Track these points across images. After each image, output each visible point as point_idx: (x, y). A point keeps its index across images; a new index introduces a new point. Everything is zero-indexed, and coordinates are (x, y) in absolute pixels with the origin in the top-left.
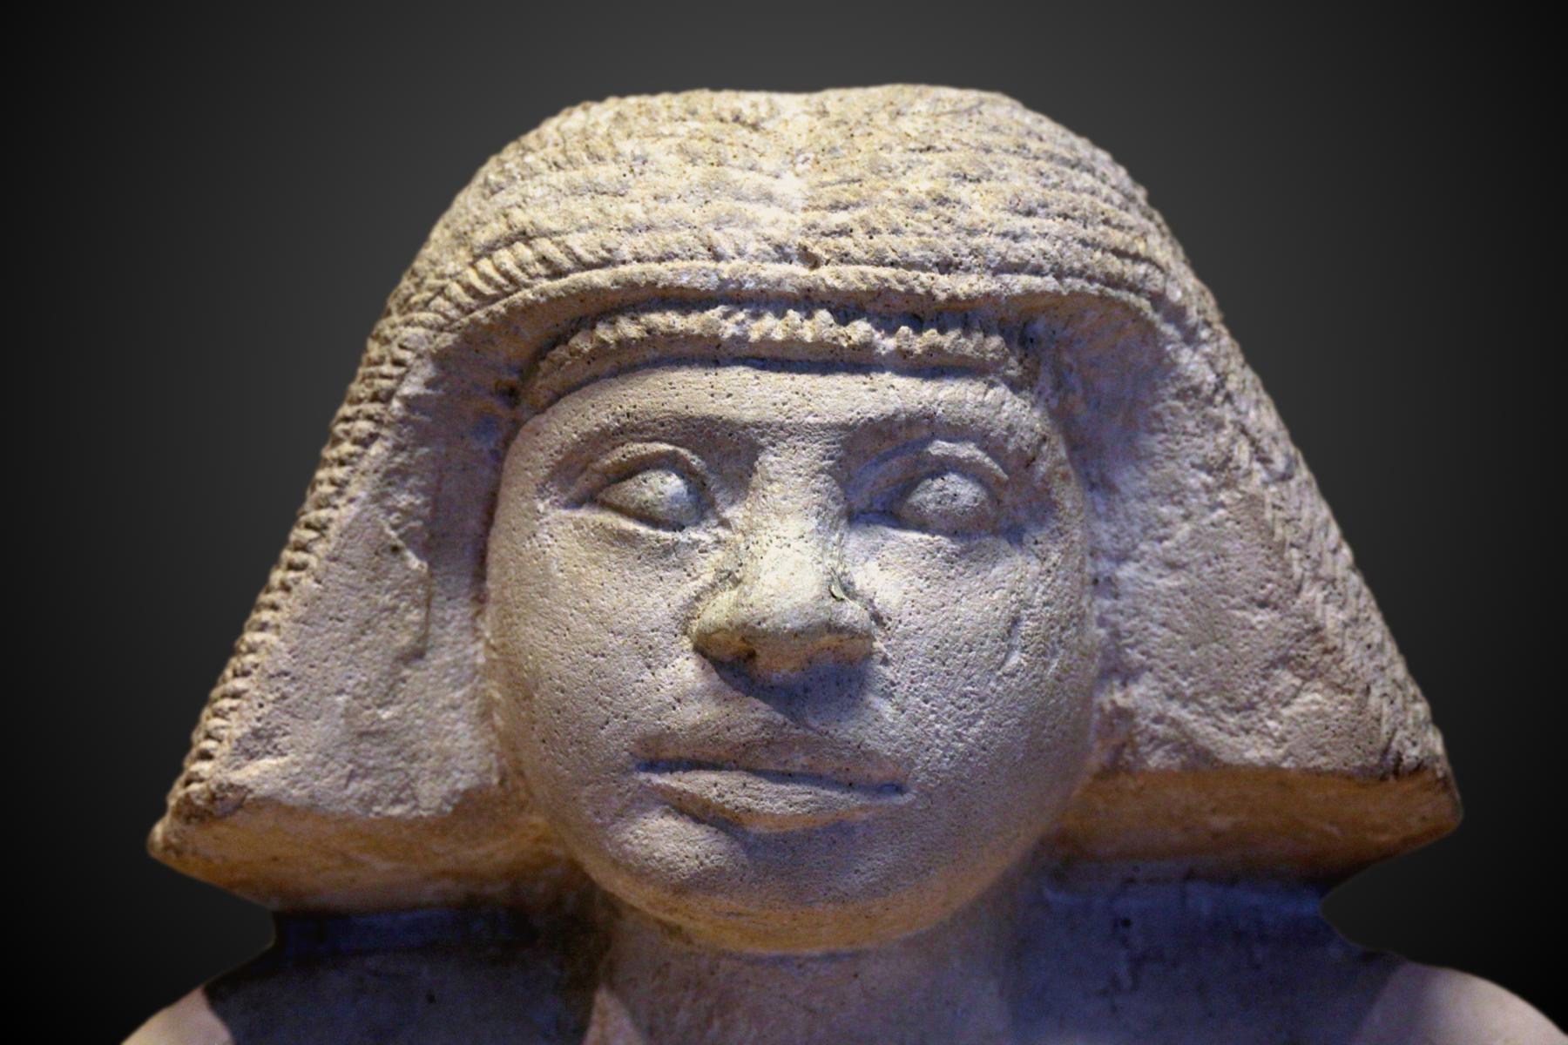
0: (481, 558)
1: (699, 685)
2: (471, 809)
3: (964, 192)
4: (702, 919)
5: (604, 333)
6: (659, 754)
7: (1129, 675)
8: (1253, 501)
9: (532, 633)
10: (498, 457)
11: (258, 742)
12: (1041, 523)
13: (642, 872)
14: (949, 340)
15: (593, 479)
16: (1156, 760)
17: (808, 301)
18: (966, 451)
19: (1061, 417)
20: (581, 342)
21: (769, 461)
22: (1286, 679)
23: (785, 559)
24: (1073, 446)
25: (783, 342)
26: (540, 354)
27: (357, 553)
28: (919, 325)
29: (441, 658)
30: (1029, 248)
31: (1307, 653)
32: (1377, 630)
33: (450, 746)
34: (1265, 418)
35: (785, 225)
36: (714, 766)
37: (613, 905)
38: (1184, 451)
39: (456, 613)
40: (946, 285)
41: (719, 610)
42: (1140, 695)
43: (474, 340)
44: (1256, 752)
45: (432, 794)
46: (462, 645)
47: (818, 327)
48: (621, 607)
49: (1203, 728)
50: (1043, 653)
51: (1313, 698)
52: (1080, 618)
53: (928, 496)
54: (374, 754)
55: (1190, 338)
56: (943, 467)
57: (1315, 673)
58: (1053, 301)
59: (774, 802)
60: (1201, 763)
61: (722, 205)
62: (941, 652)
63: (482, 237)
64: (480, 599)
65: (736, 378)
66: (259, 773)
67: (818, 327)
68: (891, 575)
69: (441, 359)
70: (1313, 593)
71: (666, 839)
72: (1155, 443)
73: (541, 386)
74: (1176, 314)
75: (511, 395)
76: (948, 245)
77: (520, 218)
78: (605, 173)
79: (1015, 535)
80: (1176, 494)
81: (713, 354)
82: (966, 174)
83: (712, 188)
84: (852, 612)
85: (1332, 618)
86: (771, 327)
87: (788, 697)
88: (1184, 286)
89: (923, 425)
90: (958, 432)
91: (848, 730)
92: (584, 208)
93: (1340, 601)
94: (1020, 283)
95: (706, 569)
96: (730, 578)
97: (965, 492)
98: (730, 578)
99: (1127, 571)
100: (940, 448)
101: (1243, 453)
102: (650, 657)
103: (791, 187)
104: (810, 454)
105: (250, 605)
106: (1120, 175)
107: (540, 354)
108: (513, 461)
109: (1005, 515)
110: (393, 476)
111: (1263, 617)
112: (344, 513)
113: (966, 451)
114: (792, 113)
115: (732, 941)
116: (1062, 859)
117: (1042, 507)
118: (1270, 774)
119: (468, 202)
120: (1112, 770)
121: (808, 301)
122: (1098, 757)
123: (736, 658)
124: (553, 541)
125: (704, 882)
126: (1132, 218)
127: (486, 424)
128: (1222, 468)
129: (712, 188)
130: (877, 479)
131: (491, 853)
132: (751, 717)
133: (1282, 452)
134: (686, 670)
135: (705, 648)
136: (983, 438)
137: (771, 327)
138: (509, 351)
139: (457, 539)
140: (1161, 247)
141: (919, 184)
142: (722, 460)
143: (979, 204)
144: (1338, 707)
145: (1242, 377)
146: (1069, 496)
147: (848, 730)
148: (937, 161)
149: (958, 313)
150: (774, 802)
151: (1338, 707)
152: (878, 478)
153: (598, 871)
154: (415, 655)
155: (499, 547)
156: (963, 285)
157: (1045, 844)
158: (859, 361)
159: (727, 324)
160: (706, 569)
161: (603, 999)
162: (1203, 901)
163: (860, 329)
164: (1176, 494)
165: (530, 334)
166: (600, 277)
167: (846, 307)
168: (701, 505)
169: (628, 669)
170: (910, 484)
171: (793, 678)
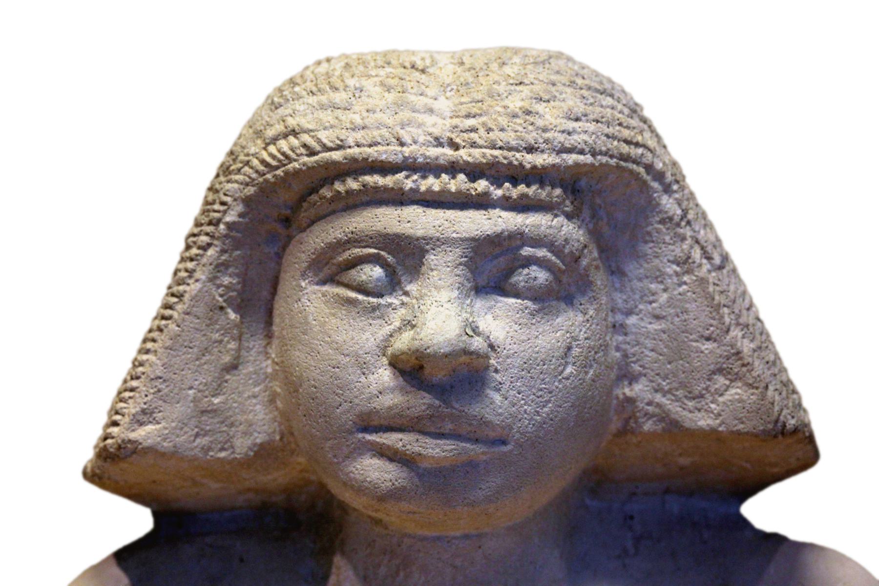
0: (270, 313)
2: (264, 454)
3: (540, 108)
4: (393, 516)
5: (339, 187)
6: (369, 423)
7: (633, 379)
8: (703, 281)
9: (298, 355)
10: (279, 256)
13: (360, 489)
14: (532, 190)
15: (333, 268)
16: (648, 426)
17: (453, 169)
18: (541, 253)
19: (595, 234)
20: (326, 192)
21: (431, 258)
22: (721, 381)
23: (440, 313)
24: (602, 250)
25: (439, 192)
26: (303, 199)
27: (200, 310)
28: (515, 182)
29: (247, 369)
30: (577, 139)
33: (252, 418)
35: (440, 126)
36: (400, 430)
37: (344, 508)
39: (256, 344)
40: (530, 160)
41: (403, 342)
42: (639, 389)
43: (266, 191)
44: (704, 422)
45: (242, 446)
46: (259, 362)
47: (458, 183)
49: (674, 408)
50: (585, 366)
51: (736, 392)
52: (605, 347)
53: (520, 278)
54: (210, 423)
56: (529, 262)
57: (737, 377)
58: (590, 169)
59: (434, 449)
60: (673, 428)
61: (405, 115)
62: (528, 366)
63: (270, 133)
64: (269, 336)
67: (458, 183)
68: (500, 323)
69: (247, 201)
70: (736, 333)
71: (373, 470)
72: (647, 249)
73: (303, 216)
75: (287, 221)
76: (531, 137)
77: (292, 122)
78: (339, 97)
79: (569, 300)
80: (659, 277)
81: (400, 198)
83: (399, 105)
84: (478, 343)
86: (432, 183)
87: (442, 391)
89: (518, 238)
90: (537, 242)
91: (476, 410)
92: (327, 117)
94: (572, 159)
95: (396, 319)
96: (409, 324)
97: (541, 276)
98: (409, 324)
99: (632, 320)
100: (527, 251)
101: (697, 254)
102: (364, 368)
103: (444, 105)
104: (454, 255)
107: (303, 199)
108: (288, 259)
109: (564, 289)
110: (220, 267)
111: (708, 346)
113: (541, 253)
115: (411, 528)
116: (596, 482)
117: (584, 284)
118: (712, 434)
120: (623, 432)
121: (453, 169)
122: (615, 425)
123: (412, 369)
124: (310, 303)
125: (394, 495)
127: (272, 238)
128: (685, 262)
129: (399, 105)
130: (491, 268)
131: (276, 478)
132: (421, 402)
134: (384, 375)
135: (395, 363)
136: (551, 246)
137: (432, 183)
138: (285, 197)
141: (515, 103)
142: (405, 258)
143: (549, 115)
144: (750, 397)
146: (599, 278)
147: (476, 410)
148: (526, 90)
149: (537, 176)
150: (434, 449)
151: (750, 397)
152: (492, 268)
153: (335, 488)
154: (233, 367)
155: (280, 307)
156: (540, 160)
157: (586, 473)
158: (482, 203)
159: (408, 182)
160: (396, 319)
161: (338, 560)
162: (674, 505)
163: (482, 185)
164: (659, 277)
165: (297, 187)
166: (337, 156)
167: (474, 172)
168: (393, 283)
169: (352, 375)
170: (510, 272)
171: (444, 380)
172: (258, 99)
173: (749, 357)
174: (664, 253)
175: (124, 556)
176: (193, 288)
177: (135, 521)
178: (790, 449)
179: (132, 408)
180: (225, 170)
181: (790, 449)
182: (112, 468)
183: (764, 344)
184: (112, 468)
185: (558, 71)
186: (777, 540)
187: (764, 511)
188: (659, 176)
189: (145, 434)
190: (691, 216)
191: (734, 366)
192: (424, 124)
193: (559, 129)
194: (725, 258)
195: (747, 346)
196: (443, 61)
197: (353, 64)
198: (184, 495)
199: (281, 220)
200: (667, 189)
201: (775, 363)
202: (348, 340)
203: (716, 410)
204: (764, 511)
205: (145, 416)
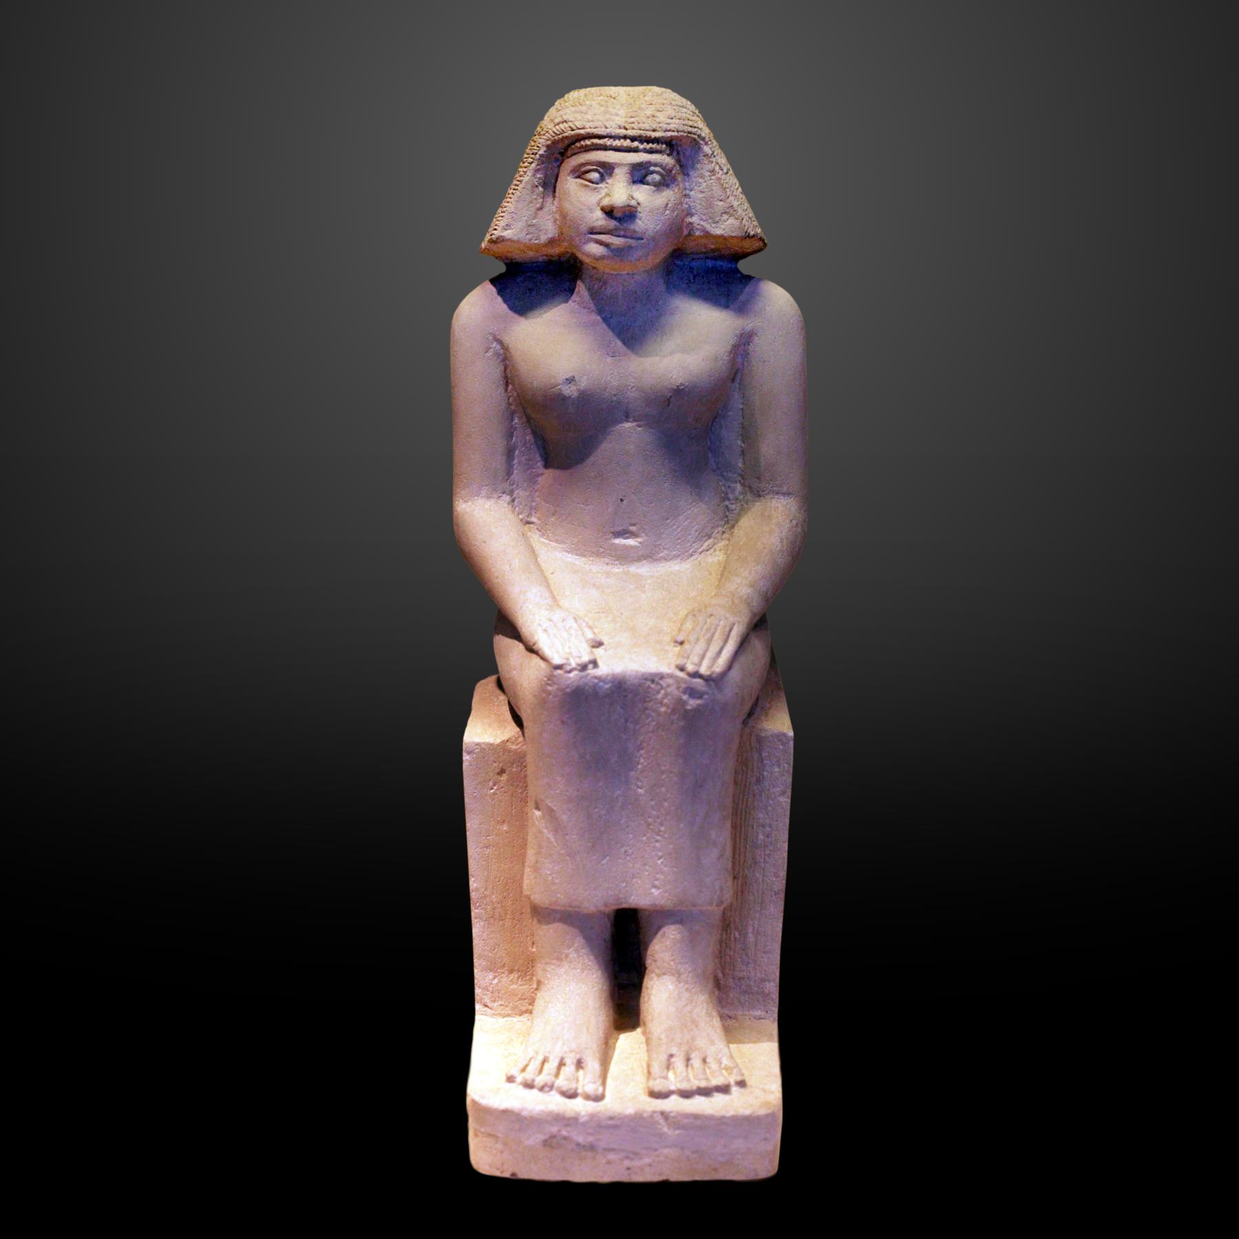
0: (555, 187)
1: (671, 987)
2: (551, 242)
3: (658, 114)
4: (600, 266)
5: (582, 143)
6: (592, 231)
7: (692, 215)
8: (719, 179)
9: (567, 206)
10: (559, 166)
11: (508, 227)
13: (588, 255)
14: (655, 146)
15: (580, 173)
16: (698, 233)
17: (625, 137)
18: (657, 169)
19: (678, 161)
20: (578, 145)
21: (617, 171)
22: (725, 217)
23: (619, 191)
24: (681, 166)
25: (578, 398)
26: (569, 146)
27: (529, 187)
28: (648, 142)
29: (545, 210)
30: (671, 127)
31: (730, 211)
32: (746, 205)
33: (548, 228)
34: (722, 160)
35: (620, 121)
36: (707, 650)
37: (581, 262)
38: (704, 167)
39: (550, 200)
40: (654, 135)
41: (606, 202)
42: (694, 219)
43: (555, 143)
44: (718, 232)
45: (544, 238)
46: (551, 206)
47: (627, 143)
48: (585, 201)
49: (708, 227)
50: (673, 211)
51: (731, 221)
52: (681, 203)
53: (649, 178)
54: (532, 230)
55: (706, 144)
56: (652, 173)
57: (732, 215)
58: (677, 137)
59: (616, 241)
60: (707, 234)
61: (608, 116)
62: (651, 211)
63: (557, 121)
64: (554, 197)
66: (507, 234)
67: (627, 143)
68: (642, 194)
69: (548, 146)
70: (732, 198)
71: (594, 249)
72: (698, 166)
73: (569, 153)
74: (703, 139)
75: (562, 154)
76: (654, 127)
77: (565, 118)
78: (583, 108)
79: (668, 186)
80: (702, 177)
81: (605, 148)
82: (655, 107)
83: (606, 112)
84: (633, 203)
85: (736, 204)
86: (617, 143)
87: (620, 220)
88: (706, 132)
89: (649, 163)
90: (656, 165)
91: (632, 227)
92: (579, 116)
93: (739, 201)
94: (669, 134)
95: (603, 192)
96: (608, 195)
97: (657, 177)
98: (608, 195)
99: (692, 193)
100: (652, 168)
101: (717, 168)
102: (591, 211)
103: (622, 112)
104: (626, 169)
105: (504, 197)
106: (693, 107)
107: (569, 146)
108: (562, 168)
109: (666, 181)
110: (537, 171)
111: (721, 203)
112: (526, 179)
113: (657, 169)
114: (621, 92)
115: (607, 271)
116: (677, 254)
117: (674, 180)
118: (721, 236)
119: (552, 111)
120: (689, 234)
121: (625, 137)
122: (686, 232)
123: (609, 212)
124: (569, 185)
125: (602, 258)
126: (695, 118)
127: (557, 160)
128: (713, 172)
129: (606, 112)
130: (639, 175)
131: (555, 251)
132: (613, 224)
133: (727, 167)
134: (599, 214)
135: (603, 209)
136: (661, 166)
137: (617, 143)
138: (561, 146)
139: (550, 184)
140: (701, 124)
141: (649, 113)
142: (607, 170)
143: (662, 117)
144: (737, 223)
145: (718, 151)
146: (680, 178)
147: (632, 227)
148: (653, 107)
149: (656, 140)
150: (616, 241)
151: (737, 223)
152: (638, 175)
153: (580, 256)
154: (541, 209)
155: (559, 185)
156: (657, 134)
157: (675, 251)
158: (636, 150)
159: (608, 142)
160: (603, 192)
161: (579, 283)
162: (710, 263)
163: (636, 144)
164: (702, 177)
165: (566, 142)
166: (582, 132)
167: (633, 139)
168: (602, 179)
169: (586, 213)
170: (646, 176)
171: (621, 216)
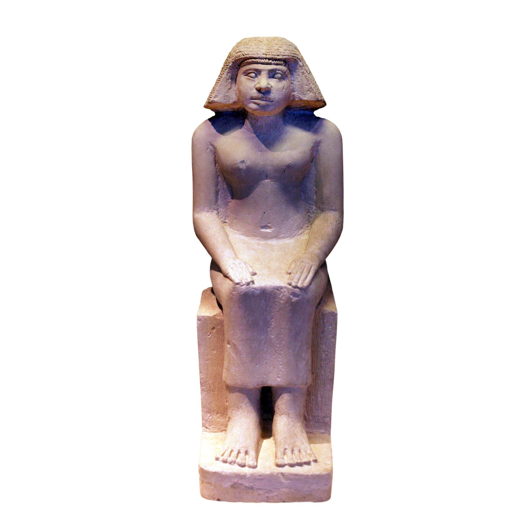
0: (236, 80)
2: (235, 103)
3: (280, 48)
4: (255, 113)
5: (248, 61)
6: (252, 98)
7: (294, 91)
8: (306, 76)
9: (241, 88)
10: (238, 71)
12: (294, 105)
13: (250, 109)
14: (278, 62)
15: (247, 73)
16: (297, 99)
17: (266, 58)
18: (280, 72)
19: (289, 68)
20: (246, 61)
21: (262, 73)
22: (309, 92)
23: (263, 81)
24: (290, 71)
25: (246, 169)
26: (242, 62)
27: (225, 79)
28: (276, 60)
29: (232, 89)
30: (286, 54)
33: (233, 97)
35: (264, 51)
37: (247, 112)
39: (234, 85)
40: (278, 57)
41: (258, 86)
42: (295, 93)
43: (236, 61)
44: (306, 99)
45: (231, 101)
46: (234, 88)
47: (267, 61)
49: (301, 97)
50: (286, 90)
51: (311, 94)
52: (290, 87)
53: (276, 76)
54: (226, 98)
56: (277, 73)
57: (311, 92)
58: (288, 58)
59: (262, 103)
60: (301, 100)
61: (258, 49)
62: (277, 90)
63: (237, 51)
64: (236, 84)
65: (255, 65)
67: (267, 61)
68: (273, 83)
69: (233, 62)
70: (311, 84)
71: (253, 106)
72: (297, 71)
73: (242, 65)
75: (239, 66)
76: (278, 54)
77: (240, 50)
78: (248, 46)
79: (284, 79)
80: (299, 75)
81: (257, 63)
83: (258, 48)
84: (269, 86)
86: (263, 61)
87: (264, 94)
89: (276, 70)
90: (279, 70)
91: (269, 96)
92: (246, 49)
94: (285, 57)
95: (257, 82)
96: (259, 83)
97: (279, 75)
98: (259, 83)
99: (294, 82)
100: (277, 72)
101: (305, 71)
102: (251, 90)
103: (264, 48)
104: (266, 72)
107: (242, 62)
108: (239, 72)
109: (283, 77)
110: (228, 73)
111: (307, 87)
113: (280, 72)
115: (258, 115)
116: (288, 108)
117: (287, 76)
118: (307, 101)
120: (293, 100)
121: (266, 58)
122: (292, 99)
123: (259, 90)
124: (242, 78)
125: (256, 110)
127: (237, 68)
128: (303, 73)
129: (258, 48)
130: (272, 74)
131: (236, 107)
132: (261, 95)
134: (255, 91)
135: (256, 89)
136: (281, 71)
137: (263, 61)
138: (238, 62)
141: (276, 48)
142: (258, 72)
143: (281, 50)
144: (313, 95)
146: (289, 76)
147: (269, 96)
148: (278, 46)
149: (279, 60)
150: (262, 103)
151: (313, 95)
152: (271, 75)
153: (247, 109)
154: (230, 89)
155: (238, 79)
156: (279, 57)
157: (287, 107)
158: (270, 64)
159: (259, 60)
160: (257, 82)
161: (246, 120)
162: (302, 112)
163: (270, 61)
164: (299, 75)
165: (241, 60)
166: (248, 56)
167: (269, 59)
168: (256, 76)
169: (249, 91)
170: (275, 75)
171: (264, 92)
172: (234, 44)
173: (314, 87)
174: (300, 71)
175: (210, 120)
176: (224, 76)
177: (213, 114)
178: (323, 104)
179: (214, 95)
180: (229, 57)
181: (323, 104)
182: (209, 105)
183: (316, 86)
184: (209, 105)
185: (283, 41)
186: (319, 118)
187: (317, 113)
188: (299, 59)
189: (216, 99)
190: (305, 65)
191: (310, 90)
192: (260, 51)
193: (283, 52)
194: (310, 72)
195: (313, 87)
196: (265, 40)
197: (250, 40)
198: (220, 109)
199: (238, 66)
200: (300, 61)
201: (318, 89)
202: (249, 85)
203: (308, 97)
204: (317, 113)
205: (216, 96)
